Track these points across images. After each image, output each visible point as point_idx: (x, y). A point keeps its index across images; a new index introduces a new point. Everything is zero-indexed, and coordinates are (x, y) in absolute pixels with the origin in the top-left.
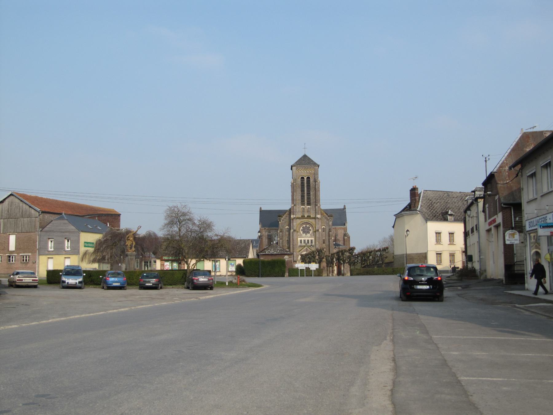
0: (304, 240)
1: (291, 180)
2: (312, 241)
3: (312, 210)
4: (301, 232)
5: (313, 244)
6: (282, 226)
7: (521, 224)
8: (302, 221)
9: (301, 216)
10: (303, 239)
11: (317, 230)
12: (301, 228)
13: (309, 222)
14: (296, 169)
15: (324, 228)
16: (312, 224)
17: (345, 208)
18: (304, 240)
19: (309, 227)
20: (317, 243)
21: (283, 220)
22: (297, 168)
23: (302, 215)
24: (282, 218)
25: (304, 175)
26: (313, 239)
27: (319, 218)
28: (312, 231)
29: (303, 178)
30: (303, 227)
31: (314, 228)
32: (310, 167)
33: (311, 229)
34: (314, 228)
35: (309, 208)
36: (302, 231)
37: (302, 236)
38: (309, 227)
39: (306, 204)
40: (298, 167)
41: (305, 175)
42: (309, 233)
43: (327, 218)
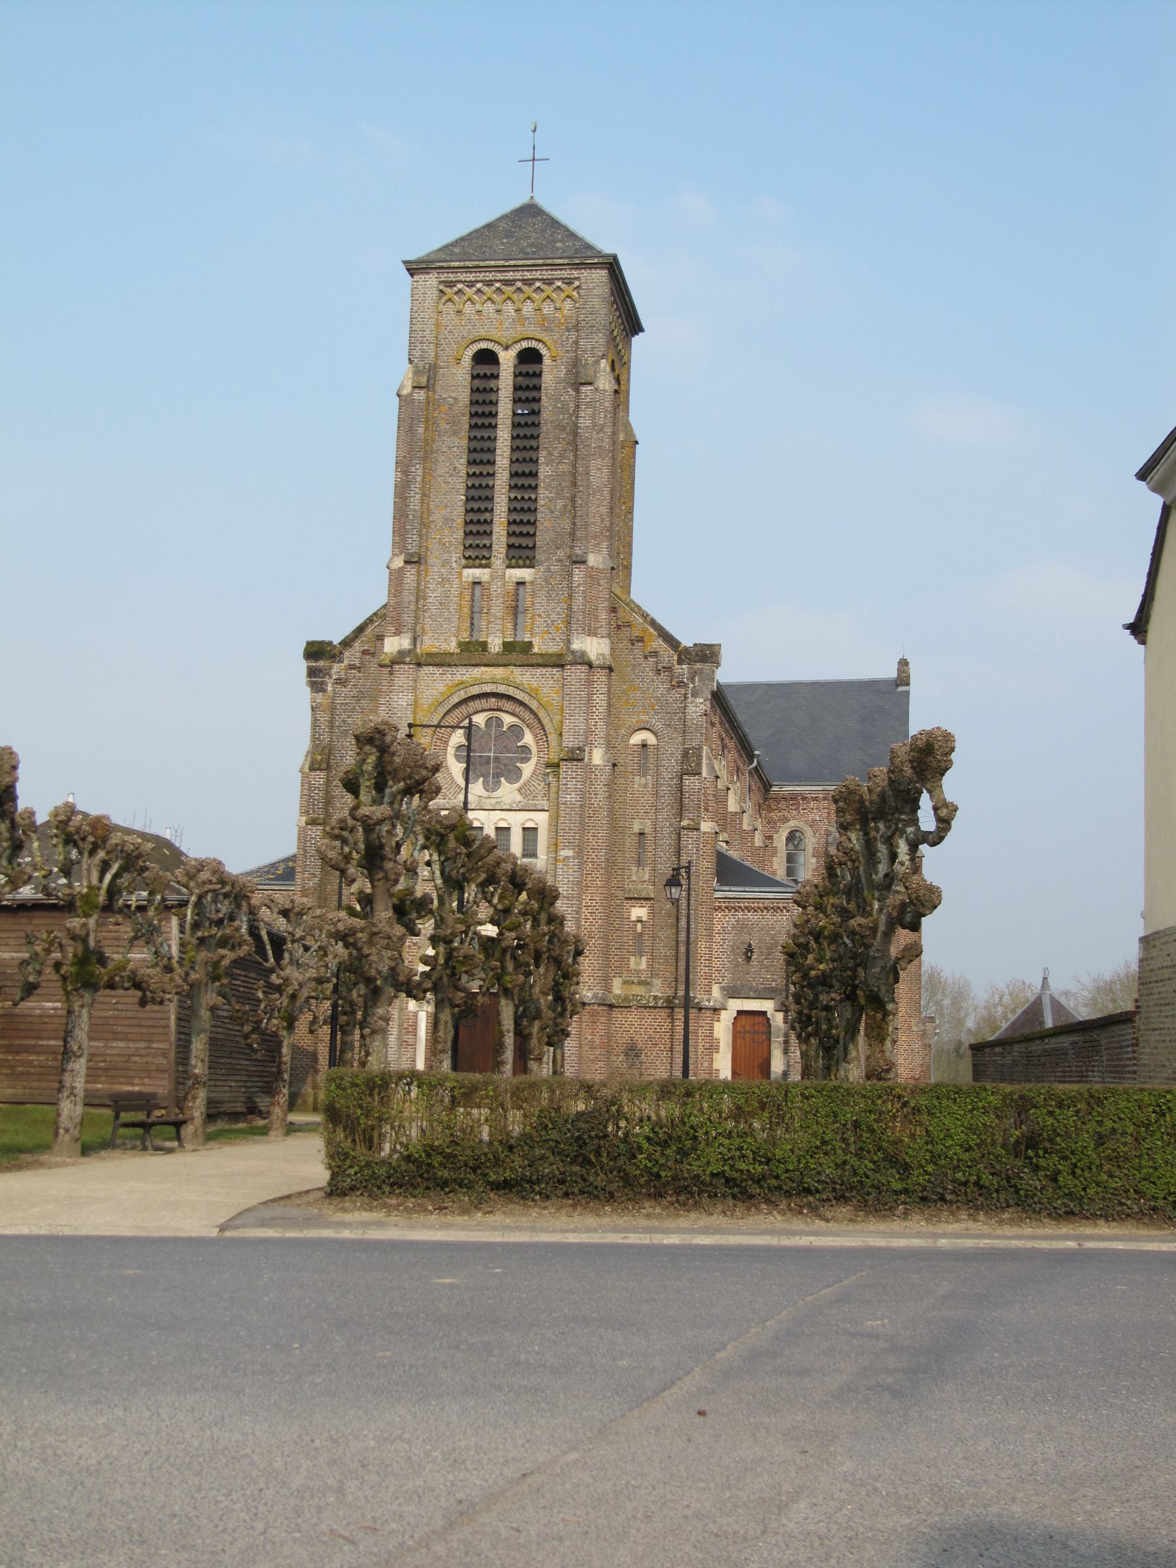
1: (400, 374)
2: (530, 833)
3: (541, 598)
6: (331, 723)
7: (162, 1023)
8: (462, 685)
9: (460, 644)
11: (572, 750)
13: (511, 691)
15: (644, 746)
16: (534, 705)
17: (903, 679)
19: (516, 731)
21: (340, 682)
22: (450, 284)
23: (465, 636)
24: (336, 667)
25: (495, 335)
26: (541, 820)
27: (590, 665)
28: (534, 760)
29: (486, 358)
31: (552, 738)
32: (547, 275)
33: (534, 749)
34: (552, 738)
35: (521, 583)
38: (512, 727)
39: (503, 550)
40: (452, 277)
41: (505, 336)
42: (514, 774)
43: (669, 669)
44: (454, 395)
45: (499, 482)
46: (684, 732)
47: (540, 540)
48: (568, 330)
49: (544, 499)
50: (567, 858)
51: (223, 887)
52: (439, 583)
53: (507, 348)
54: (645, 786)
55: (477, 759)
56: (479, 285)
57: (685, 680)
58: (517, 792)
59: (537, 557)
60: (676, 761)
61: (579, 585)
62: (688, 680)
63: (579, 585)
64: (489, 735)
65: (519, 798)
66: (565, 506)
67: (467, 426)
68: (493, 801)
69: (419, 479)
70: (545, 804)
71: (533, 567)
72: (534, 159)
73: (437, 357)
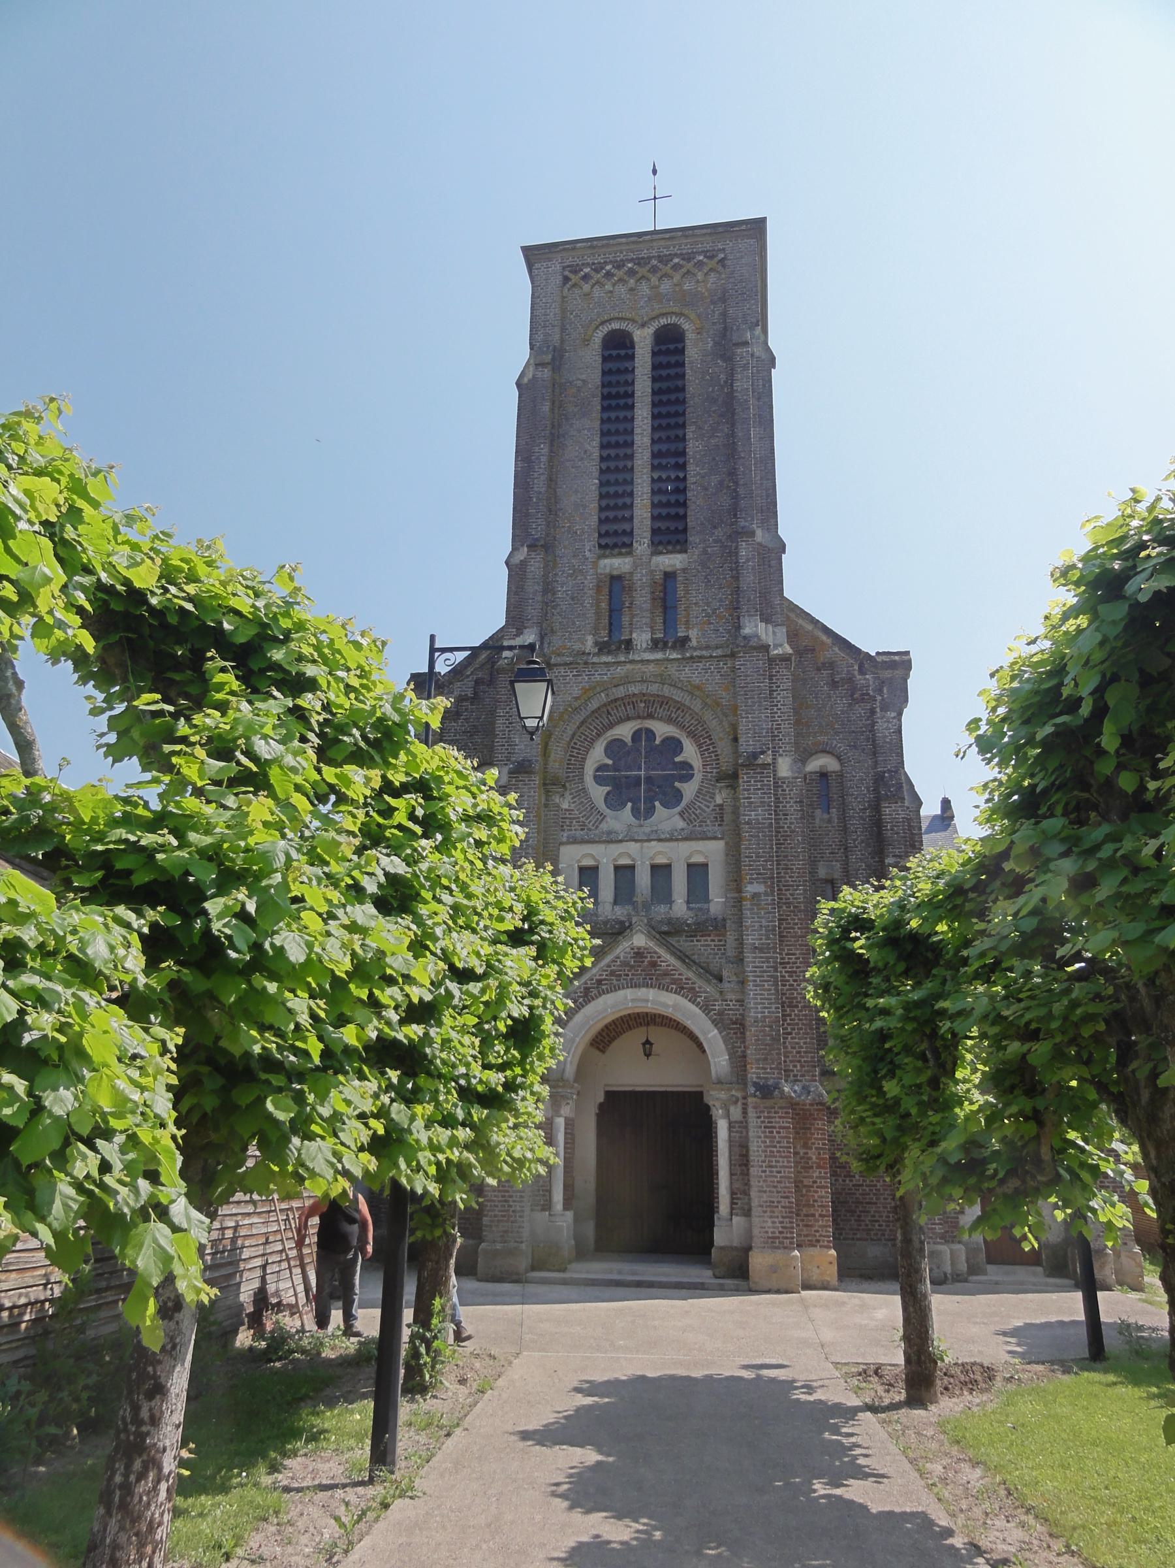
0: (655, 868)
4: (598, 793)
5: (717, 901)
10: (606, 857)
12: (597, 755)
14: (566, 279)
18: (655, 868)
19: (673, 745)
20: (751, 889)
26: (712, 851)
30: (614, 748)
36: (599, 780)
37: (604, 826)
42: (673, 798)
44: (583, 377)
45: (639, 462)
46: (874, 753)
47: (691, 521)
48: (713, 302)
49: (695, 476)
50: (755, 896)
51: (179, 847)
52: (571, 575)
53: (643, 325)
54: (829, 821)
55: (623, 780)
56: (608, 267)
57: (871, 693)
58: (677, 817)
59: (690, 539)
60: (868, 788)
61: (748, 560)
62: (874, 691)
63: (748, 560)
64: (639, 751)
65: (681, 824)
66: (721, 483)
67: (599, 408)
68: (647, 830)
69: (543, 459)
70: (717, 830)
71: (686, 552)
72: (655, 198)
73: (562, 341)
